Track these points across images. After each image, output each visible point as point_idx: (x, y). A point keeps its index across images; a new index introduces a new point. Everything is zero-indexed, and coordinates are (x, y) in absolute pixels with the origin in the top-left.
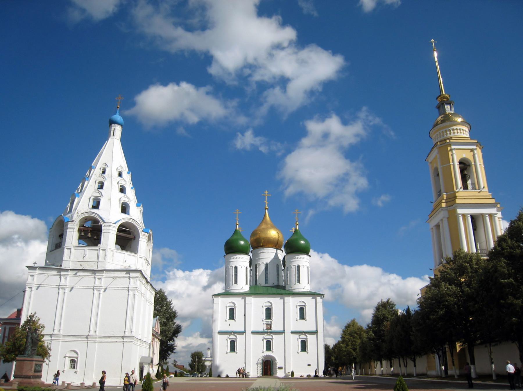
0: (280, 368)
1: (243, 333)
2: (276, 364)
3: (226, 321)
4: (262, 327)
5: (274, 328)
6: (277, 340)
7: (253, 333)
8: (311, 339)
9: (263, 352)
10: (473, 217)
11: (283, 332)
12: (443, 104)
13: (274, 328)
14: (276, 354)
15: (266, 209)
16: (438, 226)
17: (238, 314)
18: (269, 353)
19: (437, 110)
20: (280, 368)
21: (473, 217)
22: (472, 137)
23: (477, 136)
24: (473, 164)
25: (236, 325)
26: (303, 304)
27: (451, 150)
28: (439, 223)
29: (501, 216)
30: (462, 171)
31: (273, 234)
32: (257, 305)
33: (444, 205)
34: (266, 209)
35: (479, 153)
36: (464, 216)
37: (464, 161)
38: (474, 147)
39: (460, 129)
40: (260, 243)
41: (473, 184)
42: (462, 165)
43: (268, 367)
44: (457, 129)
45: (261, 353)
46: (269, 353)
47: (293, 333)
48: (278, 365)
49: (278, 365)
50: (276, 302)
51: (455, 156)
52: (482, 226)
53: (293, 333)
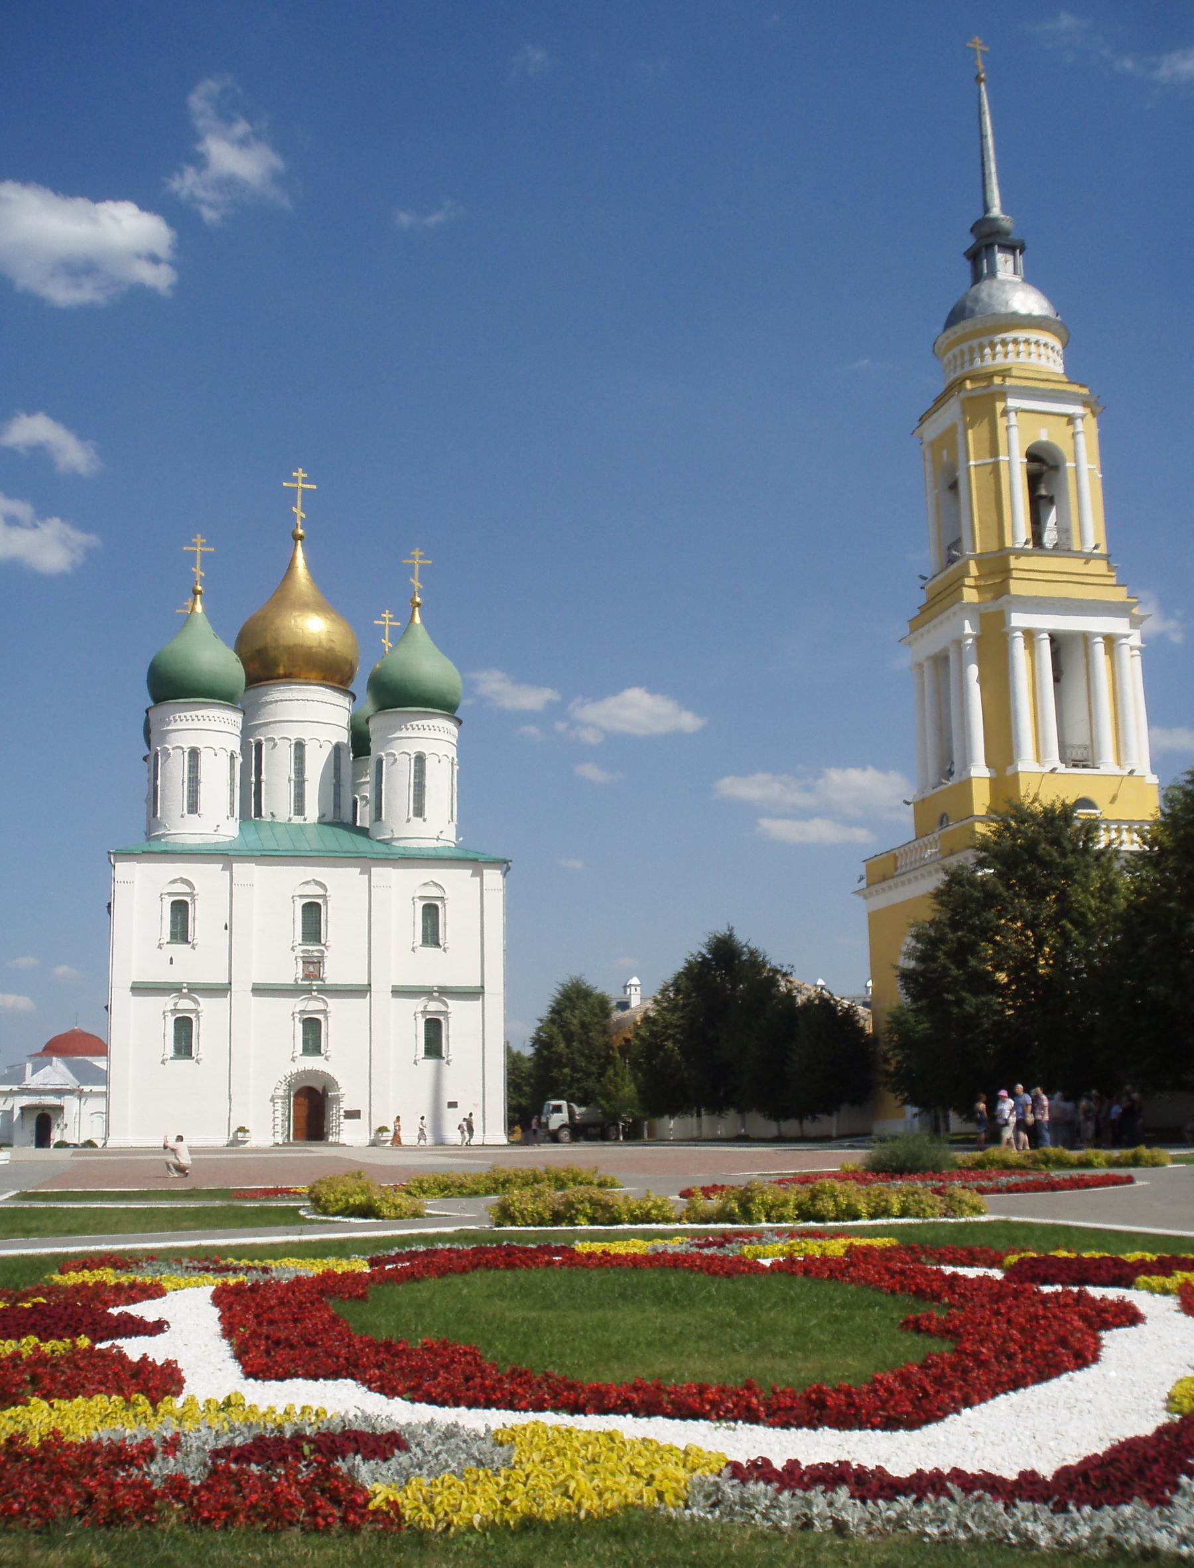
0: (353, 1115)
1: (222, 990)
2: (337, 1099)
3: (160, 947)
4: (290, 972)
5: (333, 974)
6: (340, 1017)
7: (260, 990)
8: (461, 1020)
9: (293, 1060)
10: (1054, 638)
11: (362, 991)
12: (989, 247)
13: (333, 974)
14: (339, 1064)
15: (297, 538)
16: (941, 661)
17: (202, 921)
18: (313, 1063)
19: (967, 265)
20: (353, 1115)
21: (1054, 638)
22: (1073, 372)
23: (1093, 369)
24: (1070, 464)
25: (194, 964)
26: (435, 892)
27: (1005, 413)
28: (946, 649)
29: (1138, 643)
30: (1034, 481)
31: (313, 627)
32: (273, 891)
33: (970, 595)
34: (297, 538)
35: (1087, 432)
36: (1030, 635)
37: (1036, 452)
38: (1078, 410)
39: (1037, 343)
40: (277, 665)
41: (1063, 530)
42: (1036, 466)
43: (312, 1108)
44: (1016, 342)
45: (287, 1061)
46: (313, 1063)
47: (398, 992)
48: (346, 1105)
49: (346, 1105)
50: (342, 886)
51: (1014, 432)
52: (1082, 670)
53: (398, 992)
